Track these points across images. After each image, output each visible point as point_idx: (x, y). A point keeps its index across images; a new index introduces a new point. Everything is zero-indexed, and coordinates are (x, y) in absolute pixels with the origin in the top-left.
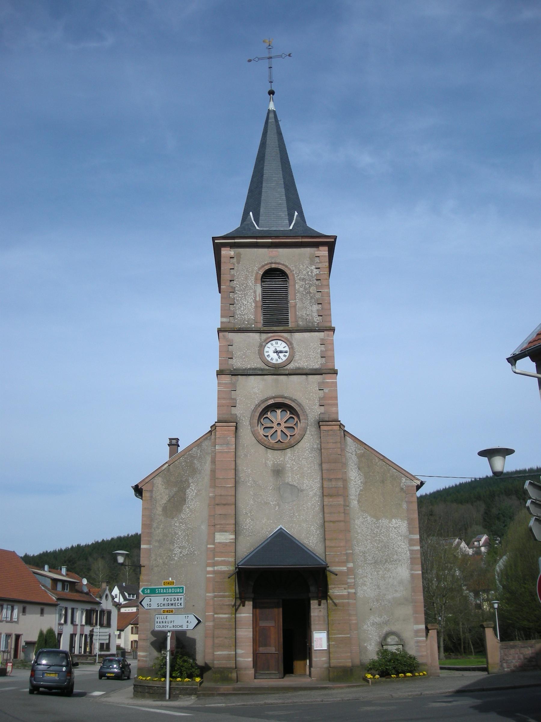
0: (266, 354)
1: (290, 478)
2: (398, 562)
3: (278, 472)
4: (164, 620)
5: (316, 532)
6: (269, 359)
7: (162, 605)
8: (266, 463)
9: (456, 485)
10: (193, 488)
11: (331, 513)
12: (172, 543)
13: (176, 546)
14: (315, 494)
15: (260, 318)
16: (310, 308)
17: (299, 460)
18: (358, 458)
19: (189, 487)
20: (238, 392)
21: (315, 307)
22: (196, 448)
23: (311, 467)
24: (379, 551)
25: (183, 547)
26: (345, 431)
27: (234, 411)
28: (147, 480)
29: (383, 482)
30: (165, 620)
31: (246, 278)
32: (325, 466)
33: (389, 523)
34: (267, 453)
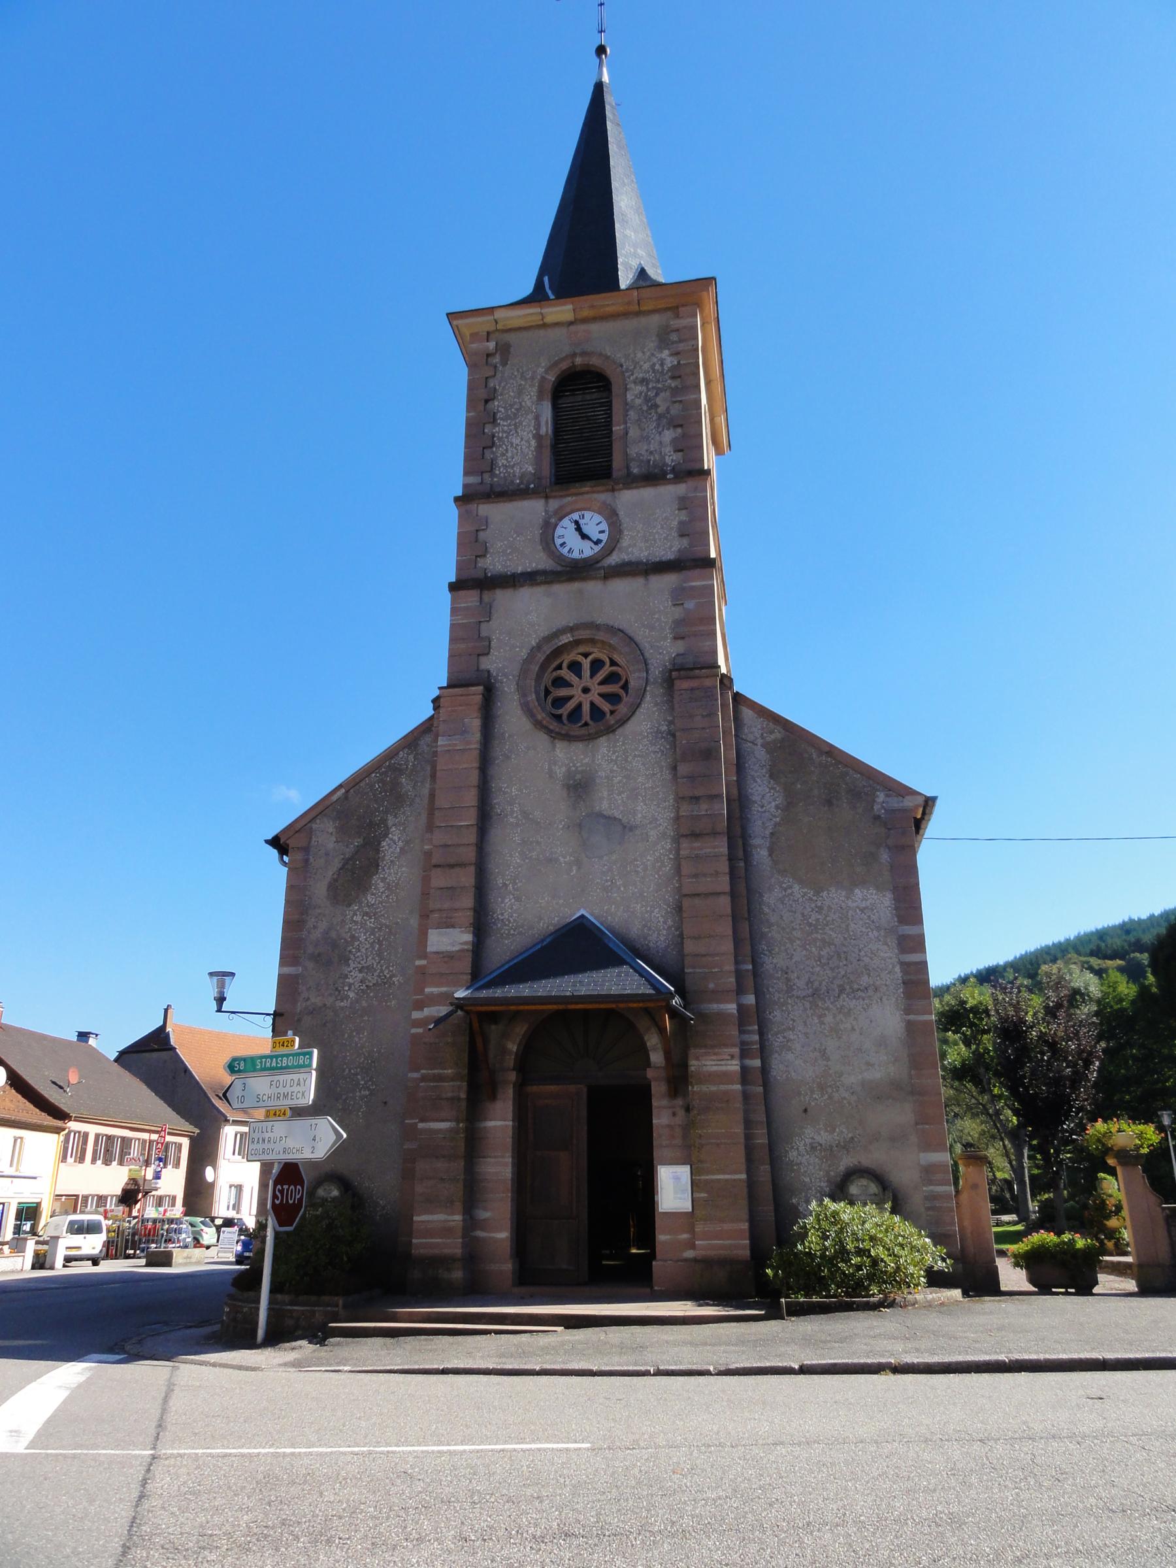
0: (558, 542)
1: (605, 801)
2: (870, 992)
3: (579, 787)
4: (266, 1136)
5: (665, 922)
6: (565, 551)
7: (265, 1098)
8: (550, 770)
9: (1152, 916)
10: (396, 838)
11: (696, 876)
12: (345, 960)
13: (352, 966)
14: (664, 834)
15: (547, 470)
16: (657, 437)
17: (626, 761)
18: (768, 752)
19: (386, 835)
20: (494, 624)
21: (668, 435)
22: (406, 750)
23: (654, 774)
24: (823, 966)
25: (367, 967)
26: (738, 697)
27: (486, 664)
28: (299, 826)
29: (829, 803)
30: (270, 1134)
31: (520, 392)
32: (683, 769)
33: (848, 898)
34: (554, 747)
